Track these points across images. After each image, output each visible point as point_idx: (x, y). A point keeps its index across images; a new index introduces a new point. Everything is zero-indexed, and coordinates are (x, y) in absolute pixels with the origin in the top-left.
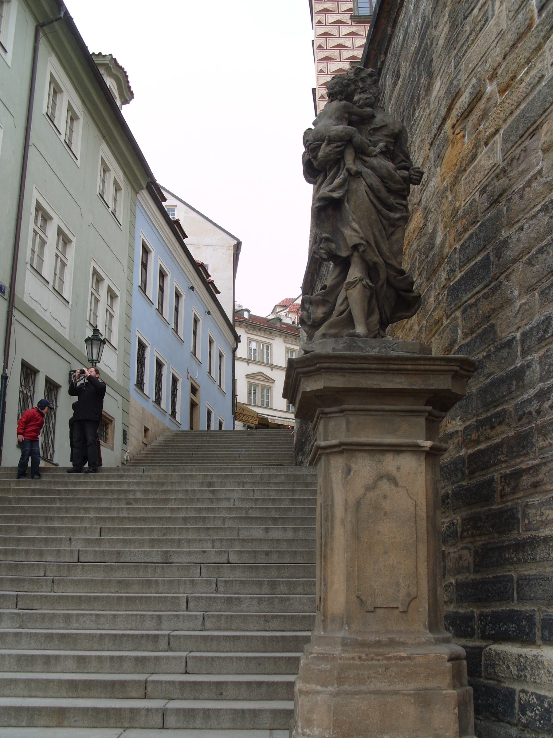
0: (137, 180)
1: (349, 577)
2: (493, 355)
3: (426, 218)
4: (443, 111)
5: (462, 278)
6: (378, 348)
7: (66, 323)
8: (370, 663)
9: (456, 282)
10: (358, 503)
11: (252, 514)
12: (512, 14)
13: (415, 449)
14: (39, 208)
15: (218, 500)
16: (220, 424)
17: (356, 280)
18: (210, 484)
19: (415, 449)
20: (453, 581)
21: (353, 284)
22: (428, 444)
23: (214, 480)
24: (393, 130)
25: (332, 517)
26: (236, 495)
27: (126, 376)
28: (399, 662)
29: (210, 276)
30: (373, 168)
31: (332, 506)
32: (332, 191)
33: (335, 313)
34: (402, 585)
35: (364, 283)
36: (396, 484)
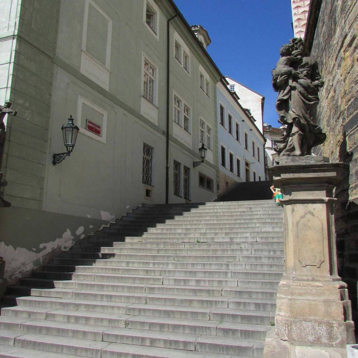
0: (216, 78)
1: (295, 252)
3: (335, 92)
4: (340, 43)
5: (348, 122)
7: (191, 144)
8: (304, 288)
9: (346, 124)
10: (298, 223)
11: (268, 221)
13: (321, 201)
14: (176, 98)
15: (253, 215)
16: (260, 178)
18: (250, 208)
19: (321, 201)
20: (348, 254)
21: (294, 134)
22: (327, 199)
23: (252, 206)
25: (288, 228)
26: (261, 213)
27: (217, 161)
28: (316, 288)
29: (251, 114)
30: (301, 84)
31: (288, 224)
32: (283, 96)
33: (288, 146)
34: (318, 256)
35: (299, 133)
36: (314, 215)
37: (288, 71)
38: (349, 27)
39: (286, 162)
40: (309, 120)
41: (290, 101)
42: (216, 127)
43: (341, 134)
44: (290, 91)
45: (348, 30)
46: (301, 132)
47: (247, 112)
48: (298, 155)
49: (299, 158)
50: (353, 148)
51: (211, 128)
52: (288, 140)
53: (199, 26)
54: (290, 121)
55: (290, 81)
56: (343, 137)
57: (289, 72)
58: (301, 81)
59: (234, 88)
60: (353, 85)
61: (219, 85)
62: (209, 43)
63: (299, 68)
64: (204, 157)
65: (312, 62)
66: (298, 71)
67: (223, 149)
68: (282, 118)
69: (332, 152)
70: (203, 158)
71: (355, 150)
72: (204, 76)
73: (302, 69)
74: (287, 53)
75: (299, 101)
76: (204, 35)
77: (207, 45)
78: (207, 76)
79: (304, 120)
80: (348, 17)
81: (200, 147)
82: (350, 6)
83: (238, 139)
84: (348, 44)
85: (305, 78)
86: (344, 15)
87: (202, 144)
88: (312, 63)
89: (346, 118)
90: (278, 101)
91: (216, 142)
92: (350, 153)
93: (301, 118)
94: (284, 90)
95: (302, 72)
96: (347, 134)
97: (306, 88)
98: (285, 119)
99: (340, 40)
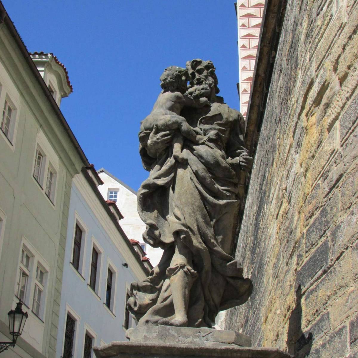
0: (73, 164)
2: (327, 344)
3: (289, 202)
4: (301, 100)
5: (307, 263)
6: (191, 337)
12: (349, 8)
17: (177, 267)
21: (174, 271)
24: (227, 118)
27: (52, 347)
30: (200, 157)
32: (158, 178)
33: (160, 300)
35: (185, 269)
37: (174, 123)
38: (317, 66)
39: (145, 336)
40: (212, 241)
41: (171, 191)
42: (60, 269)
43: (293, 290)
44: (173, 169)
45: (316, 71)
46: (190, 268)
47: (136, 248)
48: (177, 323)
49: (179, 333)
50: (313, 323)
51: (48, 269)
52: (162, 285)
53: (50, 56)
54: (168, 239)
55: (177, 147)
56: (296, 298)
57: (175, 127)
58: (201, 149)
59: (116, 197)
60: (320, 182)
61: (79, 180)
62: (67, 92)
63: (201, 122)
64: (19, 334)
65: (232, 115)
66: (197, 129)
67: (71, 321)
68: (152, 228)
69: (278, 336)
70: (15, 335)
71: (317, 328)
72: (45, 156)
73: (207, 126)
74: (177, 83)
75: (192, 194)
76: (60, 75)
77: (62, 97)
78: (52, 157)
79: (200, 240)
80: (316, 48)
81: (14, 307)
82: (321, 29)
83: (108, 303)
84: (313, 99)
85: (211, 144)
86: (311, 44)
87: (18, 301)
88: (230, 116)
89: (304, 254)
90: (145, 187)
91: (56, 302)
92: (307, 336)
93: (194, 234)
94: (162, 165)
95: (205, 132)
96: (303, 289)
97: (211, 166)
98: (157, 232)
99: (302, 93)
